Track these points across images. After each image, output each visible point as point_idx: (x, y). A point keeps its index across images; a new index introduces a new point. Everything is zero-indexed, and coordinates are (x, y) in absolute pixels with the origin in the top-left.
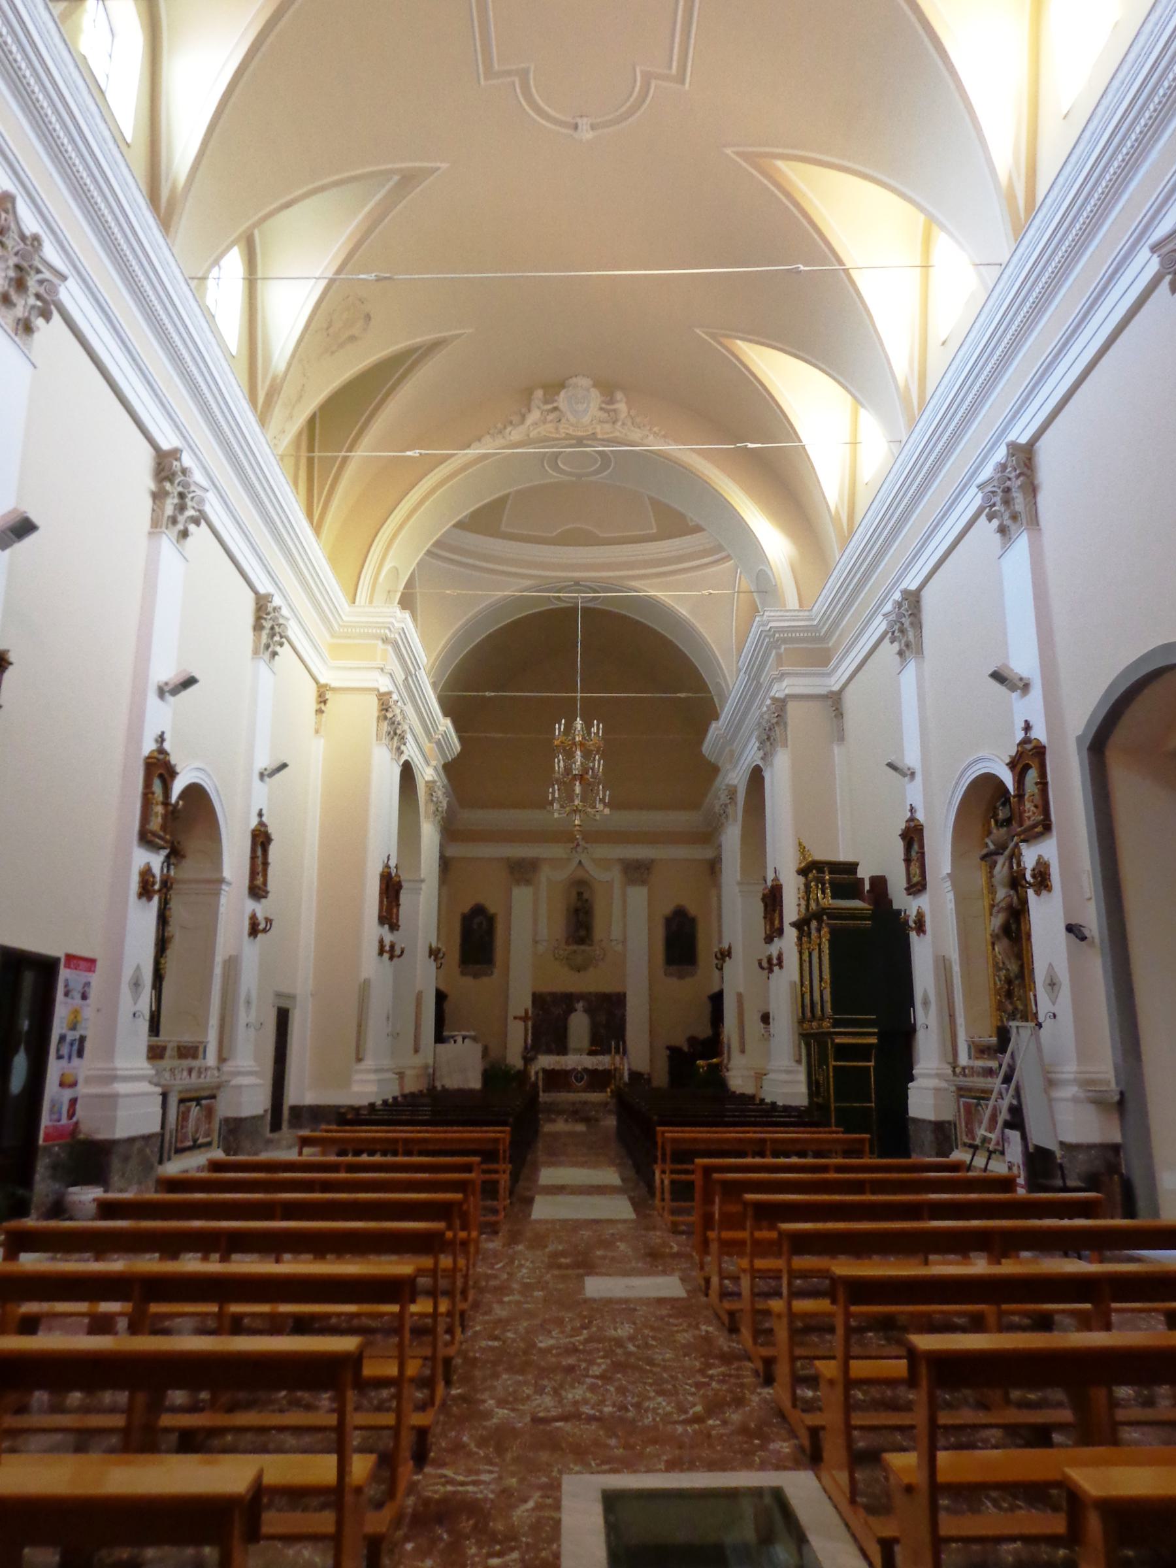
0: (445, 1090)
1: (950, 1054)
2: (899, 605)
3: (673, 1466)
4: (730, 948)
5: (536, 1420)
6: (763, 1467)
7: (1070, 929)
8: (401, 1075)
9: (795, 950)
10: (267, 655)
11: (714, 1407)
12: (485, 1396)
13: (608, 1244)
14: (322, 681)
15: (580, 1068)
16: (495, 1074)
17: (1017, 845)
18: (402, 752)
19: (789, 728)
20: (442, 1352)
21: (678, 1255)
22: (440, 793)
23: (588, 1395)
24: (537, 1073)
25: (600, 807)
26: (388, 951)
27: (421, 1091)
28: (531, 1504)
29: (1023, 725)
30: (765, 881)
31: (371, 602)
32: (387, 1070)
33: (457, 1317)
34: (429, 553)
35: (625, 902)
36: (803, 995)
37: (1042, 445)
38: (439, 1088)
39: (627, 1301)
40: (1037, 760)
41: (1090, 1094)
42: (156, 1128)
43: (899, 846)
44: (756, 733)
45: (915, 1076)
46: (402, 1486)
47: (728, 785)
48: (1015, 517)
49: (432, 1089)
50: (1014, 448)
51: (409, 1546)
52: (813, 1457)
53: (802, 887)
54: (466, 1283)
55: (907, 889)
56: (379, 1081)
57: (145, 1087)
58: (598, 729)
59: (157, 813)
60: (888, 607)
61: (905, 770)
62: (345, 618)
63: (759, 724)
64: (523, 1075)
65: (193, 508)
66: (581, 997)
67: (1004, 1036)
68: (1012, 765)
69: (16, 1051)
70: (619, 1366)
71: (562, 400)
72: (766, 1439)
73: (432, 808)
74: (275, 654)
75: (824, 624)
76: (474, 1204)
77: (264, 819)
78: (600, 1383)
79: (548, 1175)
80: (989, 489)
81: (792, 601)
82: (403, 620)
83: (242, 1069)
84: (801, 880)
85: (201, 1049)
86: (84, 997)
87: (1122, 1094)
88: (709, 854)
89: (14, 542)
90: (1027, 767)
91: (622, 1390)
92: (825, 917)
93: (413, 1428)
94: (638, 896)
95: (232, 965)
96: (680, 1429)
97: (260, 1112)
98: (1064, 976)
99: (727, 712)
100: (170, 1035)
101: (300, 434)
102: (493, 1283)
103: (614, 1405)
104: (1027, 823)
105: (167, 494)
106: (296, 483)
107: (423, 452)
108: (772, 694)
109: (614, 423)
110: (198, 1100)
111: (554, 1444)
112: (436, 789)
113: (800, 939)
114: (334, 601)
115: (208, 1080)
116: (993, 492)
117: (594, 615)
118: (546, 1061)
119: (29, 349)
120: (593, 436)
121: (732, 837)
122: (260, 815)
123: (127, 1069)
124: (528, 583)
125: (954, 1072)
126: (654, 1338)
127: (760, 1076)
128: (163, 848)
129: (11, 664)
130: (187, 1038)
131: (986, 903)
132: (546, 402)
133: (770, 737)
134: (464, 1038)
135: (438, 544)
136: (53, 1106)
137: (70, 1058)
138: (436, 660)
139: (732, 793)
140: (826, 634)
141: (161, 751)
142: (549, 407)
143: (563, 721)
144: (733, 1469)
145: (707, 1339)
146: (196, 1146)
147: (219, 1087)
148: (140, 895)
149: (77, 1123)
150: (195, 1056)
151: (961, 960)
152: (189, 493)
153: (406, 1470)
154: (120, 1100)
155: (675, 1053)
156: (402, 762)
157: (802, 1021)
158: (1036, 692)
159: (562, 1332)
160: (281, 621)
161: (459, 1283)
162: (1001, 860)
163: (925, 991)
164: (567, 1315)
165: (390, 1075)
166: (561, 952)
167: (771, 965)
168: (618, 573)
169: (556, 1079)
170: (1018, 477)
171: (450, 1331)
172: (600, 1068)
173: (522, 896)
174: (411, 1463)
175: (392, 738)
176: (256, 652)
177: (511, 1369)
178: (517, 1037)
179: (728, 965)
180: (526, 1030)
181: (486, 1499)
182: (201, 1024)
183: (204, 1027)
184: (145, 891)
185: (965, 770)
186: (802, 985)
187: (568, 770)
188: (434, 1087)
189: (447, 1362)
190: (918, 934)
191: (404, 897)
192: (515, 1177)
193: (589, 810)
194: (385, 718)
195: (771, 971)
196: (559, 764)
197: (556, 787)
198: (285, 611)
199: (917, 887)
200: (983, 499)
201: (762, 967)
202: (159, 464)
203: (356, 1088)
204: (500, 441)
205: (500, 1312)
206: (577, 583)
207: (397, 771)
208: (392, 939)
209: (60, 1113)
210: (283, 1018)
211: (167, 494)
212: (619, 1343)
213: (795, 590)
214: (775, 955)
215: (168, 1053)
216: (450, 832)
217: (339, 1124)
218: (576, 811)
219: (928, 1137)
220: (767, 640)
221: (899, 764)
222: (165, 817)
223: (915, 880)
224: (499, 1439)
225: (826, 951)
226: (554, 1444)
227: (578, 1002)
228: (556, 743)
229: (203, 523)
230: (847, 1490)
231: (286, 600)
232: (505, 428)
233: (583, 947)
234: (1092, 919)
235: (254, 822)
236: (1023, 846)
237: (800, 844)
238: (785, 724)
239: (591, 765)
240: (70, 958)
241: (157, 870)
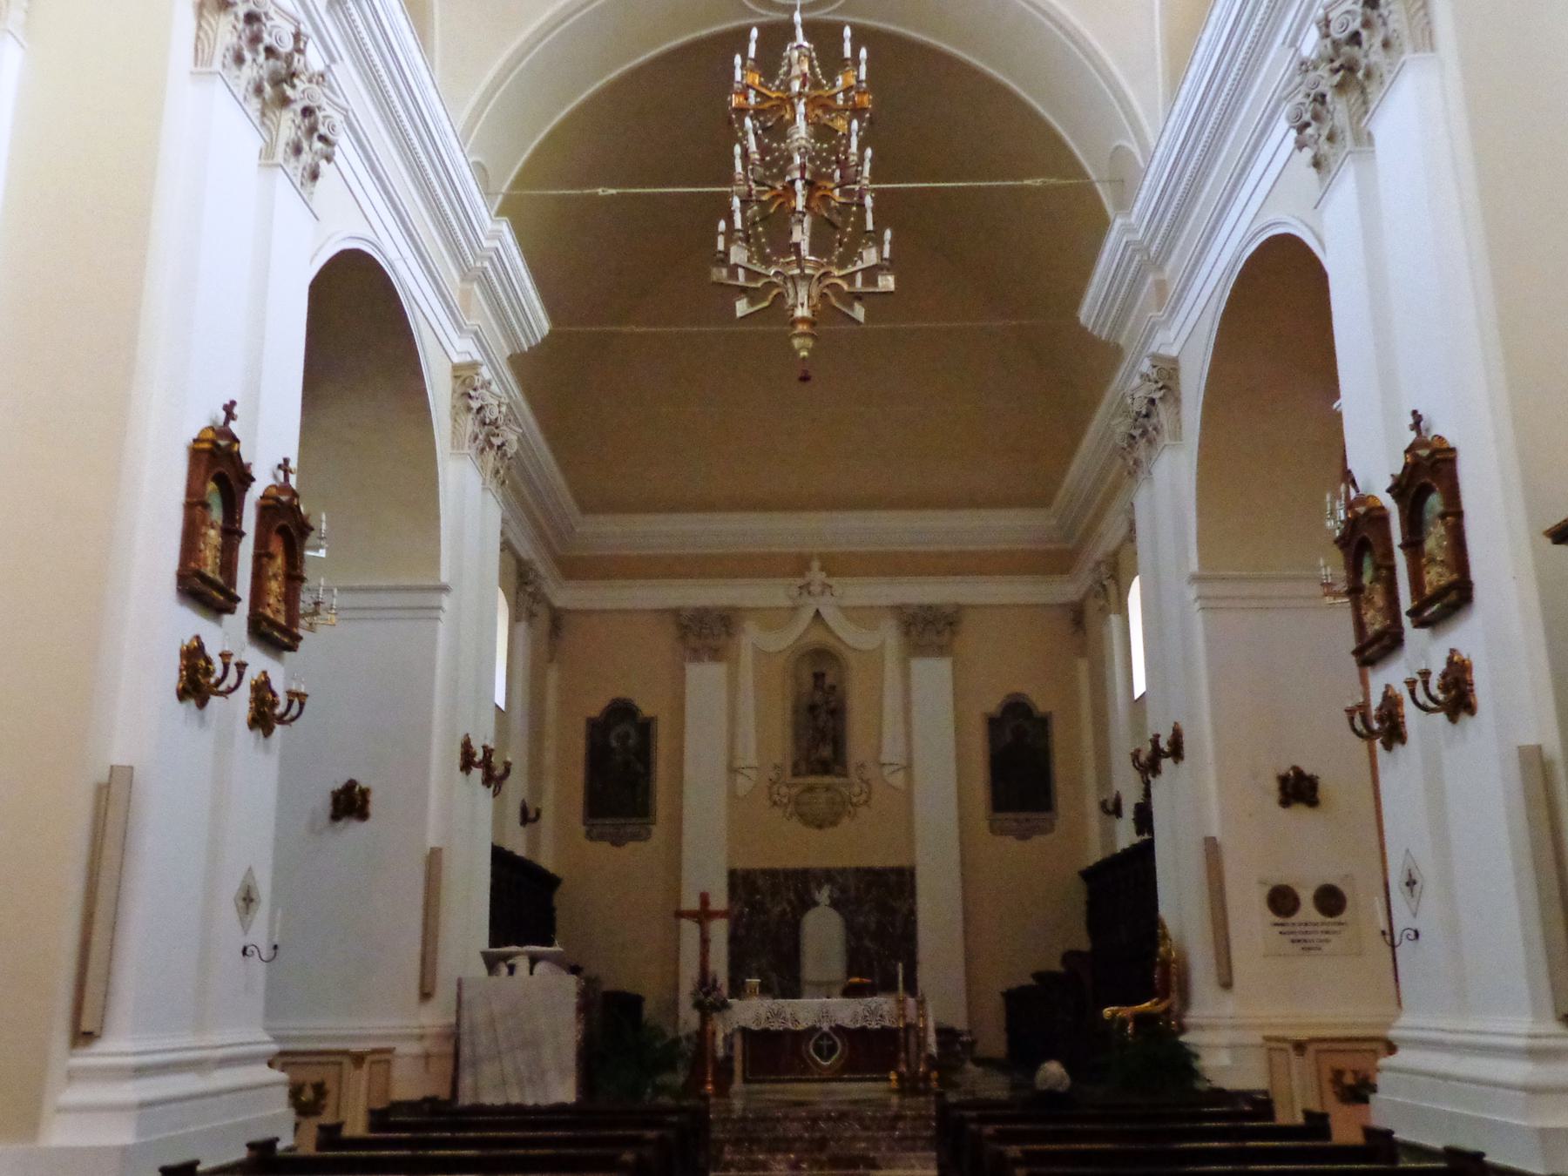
15: (825, 1027)
24: (729, 1045)
29: (1411, 421)
35: (907, 691)
44: (1287, 109)
66: (828, 876)
108: (1153, 349)
118: (752, 1011)
134: (534, 960)
166: (784, 790)
172: (874, 1025)
173: (705, 679)
220: (1137, 258)
227: (819, 887)
233: (827, 780)
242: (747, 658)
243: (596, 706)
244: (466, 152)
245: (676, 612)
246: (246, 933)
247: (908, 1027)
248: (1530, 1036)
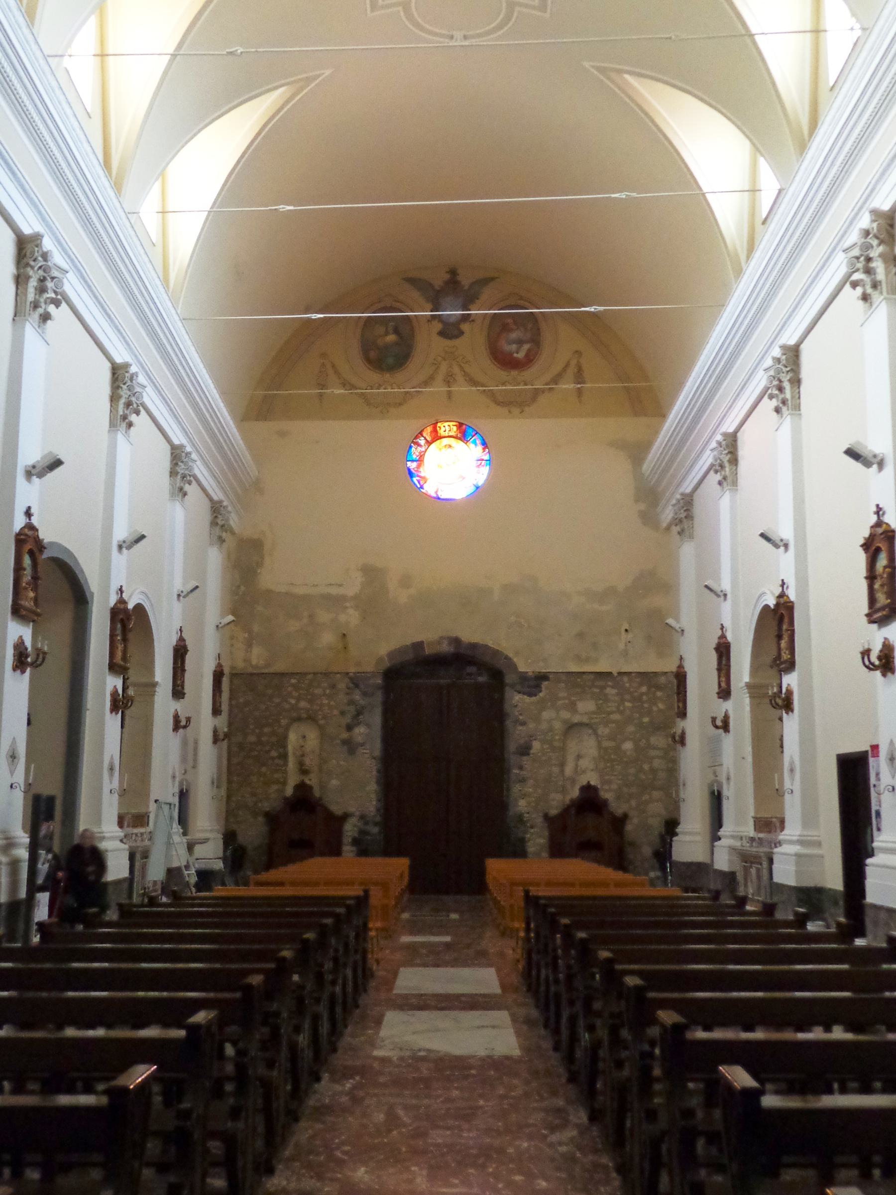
29: (875, 509)
45: (873, 849)
48: (875, 285)
74: (130, 425)
77: (35, 521)
90: (878, 550)
114: (177, 339)
141: (30, 527)
198: (142, 379)
229: (143, 412)
241: (28, 643)
244: (23, 11)
248: (733, 831)
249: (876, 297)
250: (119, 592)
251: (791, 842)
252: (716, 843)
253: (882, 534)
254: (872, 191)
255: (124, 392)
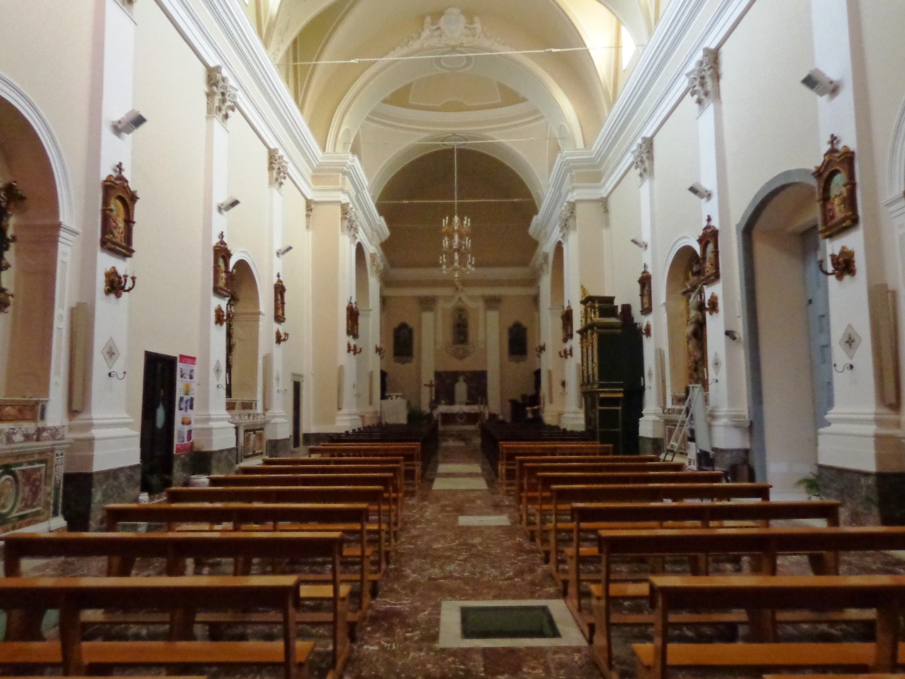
0: (386, 424)
1: (662, 401)
2: (641, 146)
3: (496, 597)
4: (544, 344)
5: (430, 579)
6: (540, 597)
7: (728, 333)
8: (362, 417)
9: (579, 346)
10: (277, 185)
11: (520, 573)
12: (406, 569)
13: (473, 501)
14: (309, 198)
16: (414, 416)
17: (702, 287)
18: (356, 238)
19: (577, 221)
20: (384, 549)
21: (507, 506)
22: (379, 260)
23: (457, 568)
25: (469, 267)
26: (353, 350)
27: (373, 425)
28: (426, 613)
29: (707, 218)
30: (563, 307)
31: (334, 150)
32: (355, 414)
33: (392, 534)
34: (368, 119)
36: (583, 371)
37: (723, 49)
38: (384, 423)
39: (479, 527)
40: (713, 239)
41: (734, 423)
42: (233, 445)
43: (638, 287)
44: (559, 222)
46: (365, 605)
47: (543, 253)
49: (380, 425)
50: (707, 51)
51: (369, 629)
52: (564, 594)
53: (583, 311)
54: (397, 519)
55: (641, 312)
56: (350, 420)
57: (226, 424)
58: (467, 222)
59: (222, 277)
60: (634, 147)
61: (642, 244)
62: (319, 160)
63: (560, 217)
64: (430, 416)
65: (230, 101)
66: (463, 373)
67: (687, 391)
68: (700, 241)
69: (157, 407)
70: (473, 556)
71: (442, 22)
72: (542, 586)
73: (375, 268)
74: (281, 184)
75: (598, 158)
76: (400, 482)
77: (225, 240)
78: (463, 563)
79: (442, 468)
80: (692, 76)
81: (580, 144)
82: (354, 161)
83: (277, 414)
84: (583, 307)
85: (254, 404)
86: (191, 378)
87: (751, 422)
88: (531, 291)
89: (134, 129)
90: (707, 243)
91: (474, 566)
92: (595, 328)
93: (370, 581)
94: (493, 316)
95: (268, 359)
96: (501, 583)
97: (288, 437)
98: (723, 358)
99: (543, 209)
100: (237, 397)
101: (287, 53)
102: (412, 519)
103: (469, 572)
104: (707, 274)
105: (215, 93)
106: (288, 82)
107: (361, 60)
108: (567, 200)
109: (473, 36)
110: (254, 431)
111: (439, 588)
112: (377, 258)
113: (582, 339)
115: (259, 420)
116: (695, 78)
117: (465, 154)
118: (443, 408)
119: (132, 15)
120: (461, 45)
121: (546, 283)
122: (278, 276)
123: (110, 419)
124: (426, 135)
125: (663, 412)
126: (492, 544)
127: (560, 415)
128: (227, 297)
129: (138, 198)
130: (247, 399)
131: (685, 320)
132: (433, 24)
133: (566, 226)
134: (397, 397)
135: (373, 113)
136: (179, 434)
137: (186, 409)
138: (373, 183)
139: (546, 256)
140: (600, 162)
141: (222, 243)
142: (434, 27)
143: (447, 218)
144: (525, 599)
145: (520, 544)
146: (255, 455)
147: (265, 423)
148: (217, 323)
149: (192, 443)
150: (251, 408)
151: (670, 352)
152: (227, 92)
153: (367, 600)
154: (213, 431)
155: (514, 403)
156: (356, 243)
157: (583, 385)
158: (715, 199)
159: (445, 541)
160: (284, 164)
161: (393, 518)
162: (693, 295)
163: (650, 368)
164: (448, 533)
165: (357, 417)
167: (566, 354)
168: (479, 128)
169: (448, 418)
170: (709, 69)
171: (388, 540)
172: (473, 412)
174: (369, 596)
175: (350, 230)
176: (270, 183)
177: (419, 556)
178: (426, 396)
179: (544, 355)
180: (431, 391)
181: (405, 611)
182: (252, 388)
183: (255, 395)
184: (219, 320)
185: (679, 239)
186: (583, 366)
187: (451, 246)
188: (381, 423)
189: (387, 553)
190: (647, 337)
191: (361, 320)
192: (424, 469)
193: (463, 269)
194: (346, 218)
195: (567, 358)
196: (446, 243)
197: (444, 256)
198: (286, 158)
199: (647, 310)
200: (689, 82)
201: (561, 356)
202: (209, 76)
203: (338, 424)
204: (406, 50)
205: (414, 532)
206: (454, 135)
207: (354, 248)
208: (355, 343)
209: (183, 438)
210: (297, 387)
211: (215, 93)
212: (474, 546)
213: (581, 136)
214: (568, 349)
215: (237, 406)
216: (386, 282)
217: (330, 442)
218: (455, 270)
219: (649, 446)
221: (638, 240)
222: (227, 279)
223: (646, 306)
224: (413, 588)
225: (596, 347)
226: (439, 588)
228: (444, 230)
229: (236, 109)
230: (577, 607)
231: (286, 152)
232: (409, 41)
234: (740, 329)
235: (275, 280)
236: (705, 287)
237: (582, 287)
238: (575, 217)
239: (464, 243)
240: (182, 357)
242: (440, 312)
243: (396, 324)
245: (419, 298)
246: (218, 380)
247: (481, 412)
249: (706, 100)
250: (118, 169)
251: (651, 414)
252: (821, 430)
253: (710, 232)
254: (642, 129)
255: (276, 166)
